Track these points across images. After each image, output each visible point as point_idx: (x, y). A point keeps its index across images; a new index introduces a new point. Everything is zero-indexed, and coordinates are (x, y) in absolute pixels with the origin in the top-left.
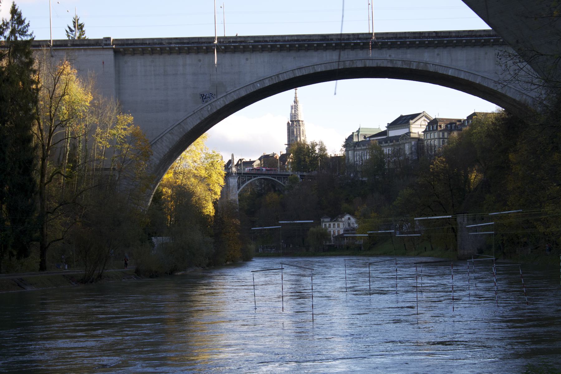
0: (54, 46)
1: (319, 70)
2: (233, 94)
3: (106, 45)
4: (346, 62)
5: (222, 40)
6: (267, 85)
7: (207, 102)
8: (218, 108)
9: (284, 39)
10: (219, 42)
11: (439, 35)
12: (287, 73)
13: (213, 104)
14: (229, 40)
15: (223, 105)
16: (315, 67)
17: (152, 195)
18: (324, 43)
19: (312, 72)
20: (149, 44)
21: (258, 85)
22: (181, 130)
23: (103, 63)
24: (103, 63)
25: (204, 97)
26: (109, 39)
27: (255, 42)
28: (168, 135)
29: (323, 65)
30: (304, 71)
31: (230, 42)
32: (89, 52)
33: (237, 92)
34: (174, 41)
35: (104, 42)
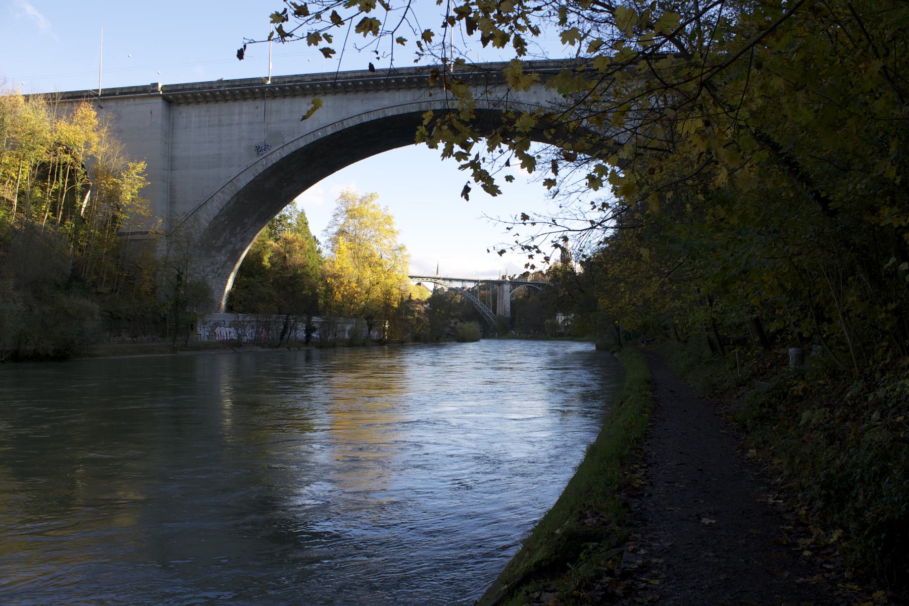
0: (102, 95)
1: (390, 114)
2: (290, 144)
3: (153, 91)
4: (422, 104)
5: (276, 81)
6: (329, 134)
7: (262, 155)
8: (274, 162)
9: (345, 76)
10: (273, 82)
11: (534, 65)
12: (353, 118)
13: (269, 157)
14: (284, 80)
15: (280, 158)
16: (386, 110)
17: (805, 578)
18: (393, 79)
19: (381, 116)
20: (199, 89)
21: (320, 134)
22: (233, 188)
23: (151, 112)
24: (151, 112)
25: (259, 150)
26: (156, 85)
27: (313, 80)
28: (219, 194)
29: (394, 108)
30: (372, 116)
31: (284, 82)
32: (138, 101)
33: (296, 143)
34: (225, 84)
35: (152, 89)
